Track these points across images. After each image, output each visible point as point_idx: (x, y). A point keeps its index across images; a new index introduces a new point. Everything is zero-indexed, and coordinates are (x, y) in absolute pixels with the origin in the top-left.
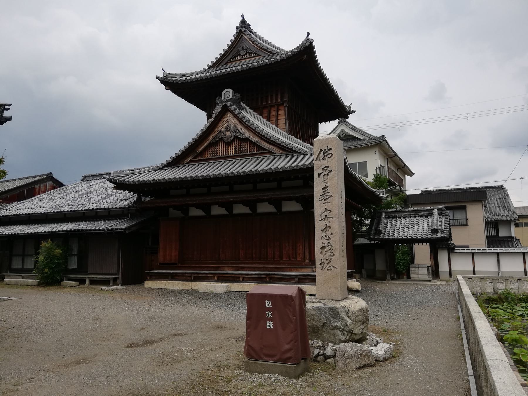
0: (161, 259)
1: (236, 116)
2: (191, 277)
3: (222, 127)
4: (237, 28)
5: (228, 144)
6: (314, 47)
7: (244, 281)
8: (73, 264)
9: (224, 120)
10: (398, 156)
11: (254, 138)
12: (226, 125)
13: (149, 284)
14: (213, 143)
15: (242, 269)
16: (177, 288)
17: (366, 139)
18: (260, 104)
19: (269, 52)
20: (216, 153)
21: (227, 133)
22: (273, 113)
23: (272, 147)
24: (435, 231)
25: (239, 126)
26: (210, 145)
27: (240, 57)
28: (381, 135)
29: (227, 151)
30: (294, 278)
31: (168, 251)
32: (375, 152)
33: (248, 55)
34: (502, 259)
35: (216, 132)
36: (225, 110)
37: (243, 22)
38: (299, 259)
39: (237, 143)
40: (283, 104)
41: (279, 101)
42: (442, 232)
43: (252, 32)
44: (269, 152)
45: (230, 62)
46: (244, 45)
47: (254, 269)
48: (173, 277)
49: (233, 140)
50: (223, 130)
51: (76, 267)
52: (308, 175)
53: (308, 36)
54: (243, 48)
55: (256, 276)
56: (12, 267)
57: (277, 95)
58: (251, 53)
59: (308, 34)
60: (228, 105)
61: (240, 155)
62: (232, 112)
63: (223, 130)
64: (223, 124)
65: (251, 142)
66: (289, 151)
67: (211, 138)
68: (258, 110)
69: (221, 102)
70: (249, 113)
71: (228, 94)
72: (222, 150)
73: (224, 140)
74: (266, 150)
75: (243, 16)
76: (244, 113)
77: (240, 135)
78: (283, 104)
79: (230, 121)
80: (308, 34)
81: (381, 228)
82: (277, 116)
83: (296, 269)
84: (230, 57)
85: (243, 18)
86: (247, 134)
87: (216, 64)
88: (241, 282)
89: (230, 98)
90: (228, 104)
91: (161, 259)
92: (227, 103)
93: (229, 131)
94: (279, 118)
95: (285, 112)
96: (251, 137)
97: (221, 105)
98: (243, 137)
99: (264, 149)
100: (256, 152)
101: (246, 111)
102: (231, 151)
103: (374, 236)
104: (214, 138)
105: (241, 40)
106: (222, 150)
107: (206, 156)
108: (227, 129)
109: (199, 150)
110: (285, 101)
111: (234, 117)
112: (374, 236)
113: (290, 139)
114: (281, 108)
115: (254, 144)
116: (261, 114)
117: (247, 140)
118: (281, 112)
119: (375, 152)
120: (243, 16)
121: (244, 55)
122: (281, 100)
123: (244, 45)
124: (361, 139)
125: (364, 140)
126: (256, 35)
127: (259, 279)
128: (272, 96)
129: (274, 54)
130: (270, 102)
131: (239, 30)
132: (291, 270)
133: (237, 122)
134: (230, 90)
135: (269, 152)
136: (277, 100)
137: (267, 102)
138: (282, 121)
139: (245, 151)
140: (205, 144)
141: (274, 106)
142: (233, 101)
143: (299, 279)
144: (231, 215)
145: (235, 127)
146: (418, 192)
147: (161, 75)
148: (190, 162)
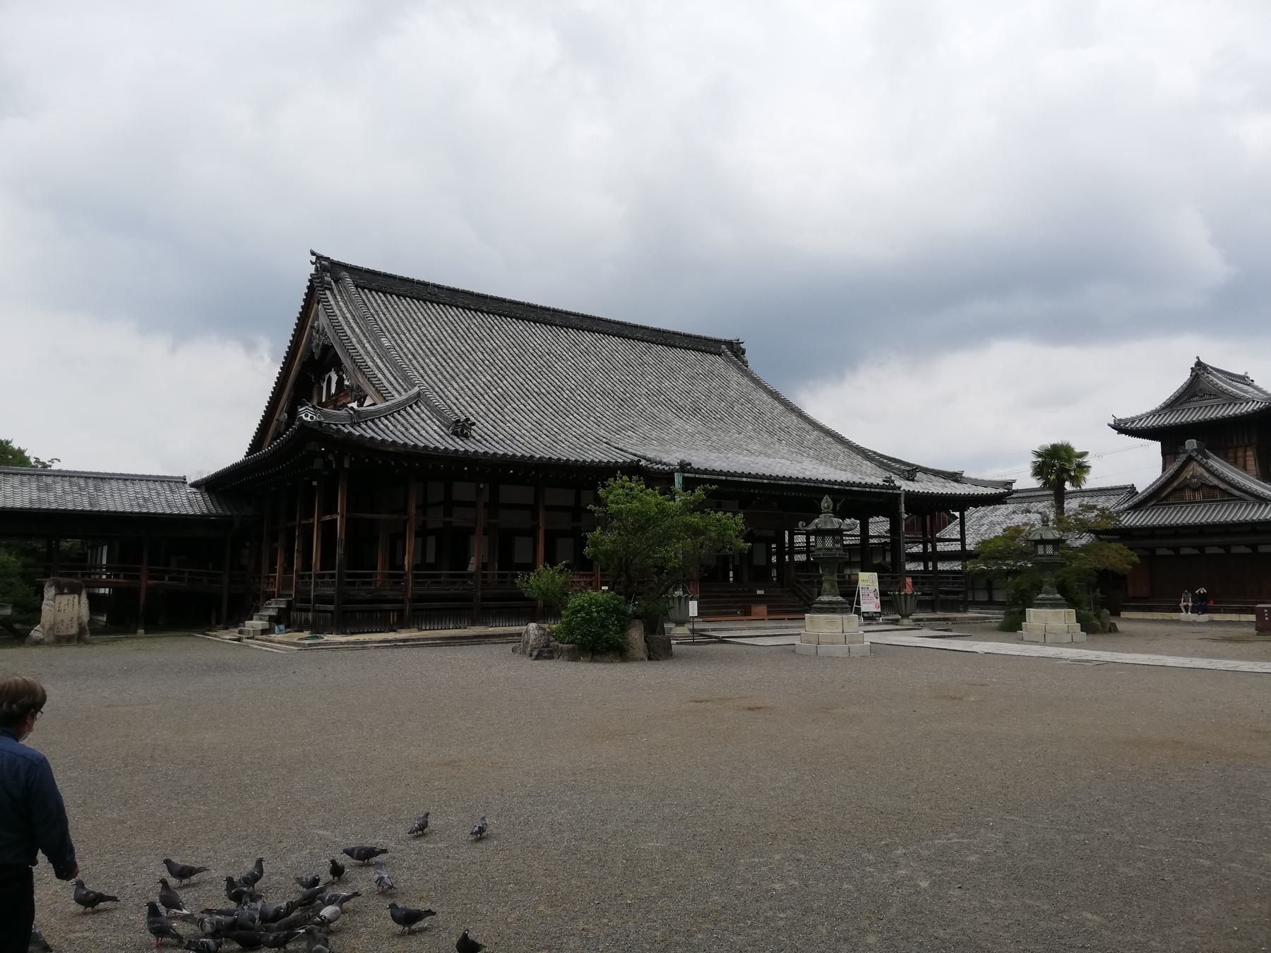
1: (1201, 465)
2: (990, 588)
3: (1187, 474)
5: (1195, 490)
11: (1223, 486)
15: (1221, 602)
22: (1240, 454)
25: (1206, 475)
26: (1175, 490)
35: (1181, 479)
36: (1190, 459)
44: (1240, 499)
45: (1185, 402)
46: (1201, 386)
48: (1150, 609)
67: (1175, 484)
69: (1185, 452)
72: (1188, 494)
76: (1211, 462)
79: (1195, 469)
82: (1245, 457)
86: (1216, 482)
87: (1173, 404)
90: (1194, 454)
99: (1231, 495)
102: (1199, 496)
108: (1193, 477)
115: (1224, 491)
117: (1216, 487)
118: (1250, 453)
123: (1201, 386)
135: (1240, 499)
138: (1251, 463)
142: (1199, 451)
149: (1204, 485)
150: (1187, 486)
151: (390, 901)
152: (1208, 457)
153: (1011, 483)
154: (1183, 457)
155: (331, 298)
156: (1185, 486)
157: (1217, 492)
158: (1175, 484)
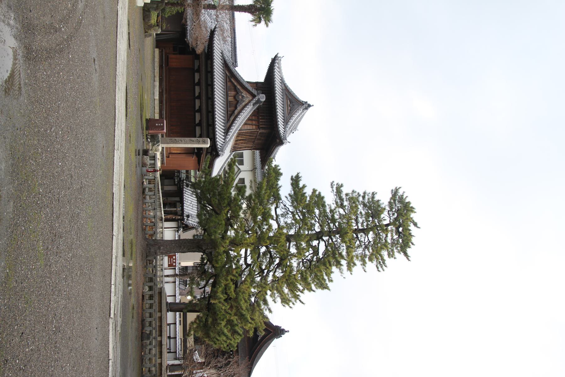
0: (171, 56)
3: (244, 93)
7: (160, 106)
9: (248, 95)
11: (236, 112)
13: (157, 51)
20: (230, 90)
22: (254, 122)
24: (188, 216)
25: (243, 104)
26: (235, 86)
27: (289, 103)
29: (230, 96)
31: (176, 61)
34: (173, 284)
35: (242, 90)
36: (254, 96)
37: (309, 106)
42: (188, 220)
44: (228, 120)
49: (236, 100)
57: (265, 125)
61: (228, 104)
62: (252, 100)
64: (246, 94)
66: (227, 131)
67: (239, 87)
69: (258, 94)
72: (232, 93)
77: (239, 104)
84: (290, 97)
86: (239, 108)
91: (171, 56)
97: (256, 94)
101: (253, 108)
102: (231, 99)
106: (232, 93)
107: (229, 84)
108: (243, 97)
109: (232, 80)
117: (236, 108)
135: (228, 120)
136: (261, 125)
139: (230, 107)
140: (236, 84)
142: (258, 101)
144: (195, 98)
145: (244, 101)
146: (275, 324)
147: (279, 56)
150: (237, 93)
152: (254, 105)
154: (255, 92)
158: (239, 87)
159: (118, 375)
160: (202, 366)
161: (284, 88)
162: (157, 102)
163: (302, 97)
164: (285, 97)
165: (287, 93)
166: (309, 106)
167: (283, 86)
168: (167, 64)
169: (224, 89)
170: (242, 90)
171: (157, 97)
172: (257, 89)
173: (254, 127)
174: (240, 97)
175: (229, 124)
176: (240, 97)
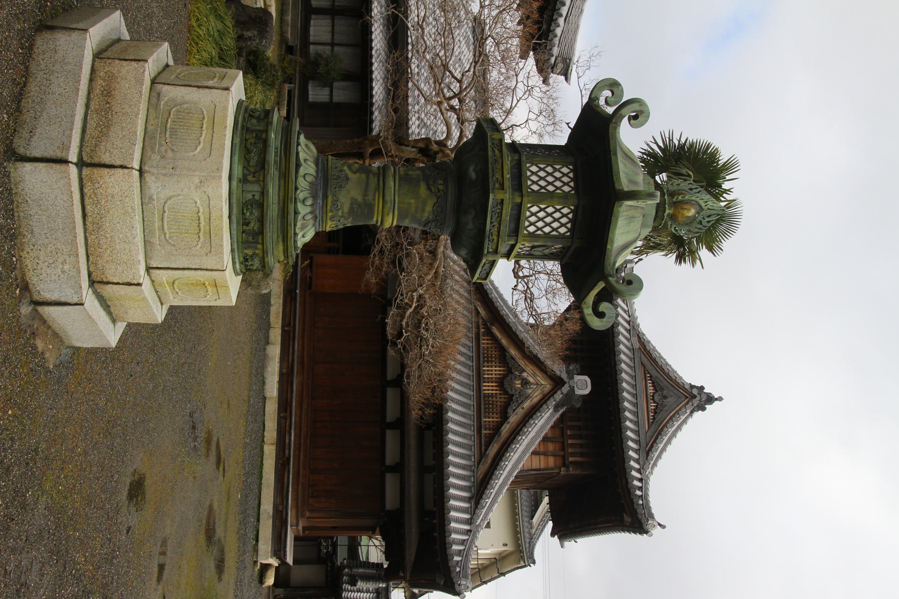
3: (530, 373)
4: (702, 388)
5: (500, 383)
6: (640, 533)
8: (317, 94)
10: (499, 577)
11: (506, 429)
12: (531, 380)
14: (505, 356)
16: (272, 302)
17: (531, 528)
18: (569, 423)
19: (652, 446)
21: (519, 382)
23: (489, 461)
25: (527, 404)
26: (503, 351)
27: (651, 390)
28: (536, 558)
29: (489, 380)
30: (283, 504)
32: (505, 545)
33: (652, 406)
35: (522, 363)
37: (710, 399)
38: (311, 501)
39: (501, 400)
40: (564, 465)
41: (571, 459)
43: (692, 412)
44: (482, 455)
45: (646, 371)
47: (298, 436)
49: (505, 392)
50: (525, 375)
51: (310, 100)
52: (436, 534)
53: (660, 525)
54: (665, 397)
55: (287, 441)
56: (313, 17)
57: (582, 455)
58: (655, 413)
59: (662, 526)
60: (563, 389)
61: (481, 403)
62: (552, 393)
63: (525, 375)
64: (534, 375)
65: (500, 425)
67: (513, 352)
68: (559, 425)
70: (549, 418)
71: (583, 385)
72: (493, 371)
73: (507, 376)
74: (486, 450)
75: (720, 399)
78: (564, 465)
80: (662, 526)
81: (360, 584)
83: (295, 499)
84: (654, 373)
85: (716, 399)
86: (513, 419)
87: (645, 352)
88: (279, 414)
89: (576, 388)
90: (565, 389)
92: (566, 386)
93: (522, 386)
94: (542, 457)
95: (552, 469)
96: (508, 426)
97: (564, 376)
98: (509, 410)
99: (488, 445)
100: (484, 432)
102: (489, 388)
103: (347, 575)
104: (512, 358)
105: (679, 394)
106: (493, 371)
107: (485, 342)
108: (525, 383)
109: (496, 331)
110: (568, 470)
111: (545, 396)
112: (347, 575)
113: (507, 478)
114: (559, 461)
116: (545, 439)
117: (505, 417)
119: (505, 545)
120: (720, 399)
121: (653, 399)
122: (572, 462)
124: (532, 517)
125: (531, 524)
126: (687, 418)
127: (282, 432)
128: (581, 446)
129: (648, 455)
130: (570, 442)
131: (695, 392)
132: (296, 491)
133: (535, 400)
134: (587, 391)
136: (572, 455)
137: (571, 437)
140: (504, 342)
141: (563, 450)
143: (282, 511)
145: (528, 397)
148: (478, 313)
149: (509, 400)
150: (509, 371)
151: (171, 63)
152: (556, 408)
153: (566, 74)
154: (559, 368)
155: (548, 414)
156: (509, 368)
157: (494, 419)
158: (513, 352)
159: (378, 10)
160: (376, 573)
161: (637, 345)
162: (272, 408)
163: (688, 371)
164: (640, 373)
165: (646, 362)
166: (710, 399)
167: (635, 340)
168: (308, 285)
169: (470, 358)
170: (522, 363)
171: (272, 389)
172: (567, 360)
173: (551, 461)
174: (518, 384)
175: (483, 468)
176: (518, 384)
